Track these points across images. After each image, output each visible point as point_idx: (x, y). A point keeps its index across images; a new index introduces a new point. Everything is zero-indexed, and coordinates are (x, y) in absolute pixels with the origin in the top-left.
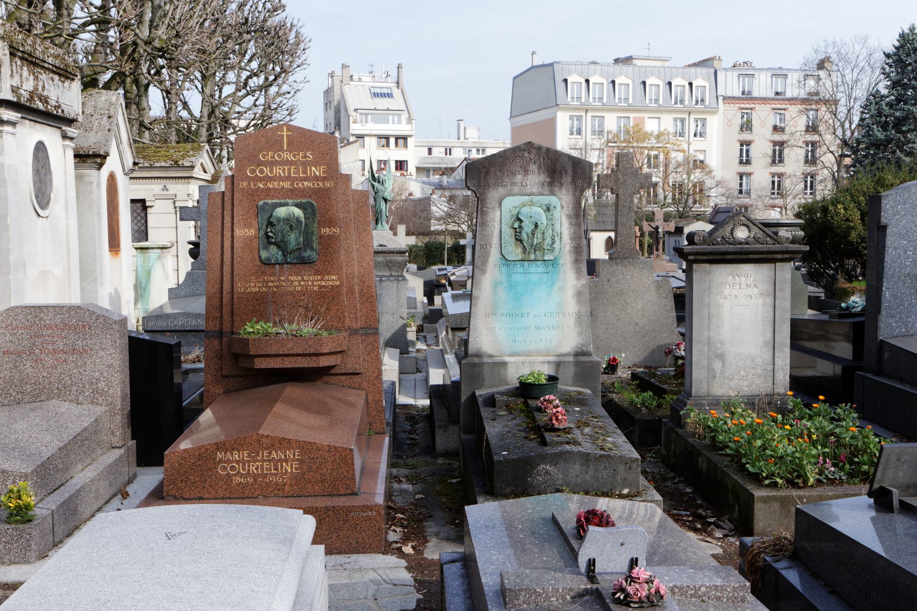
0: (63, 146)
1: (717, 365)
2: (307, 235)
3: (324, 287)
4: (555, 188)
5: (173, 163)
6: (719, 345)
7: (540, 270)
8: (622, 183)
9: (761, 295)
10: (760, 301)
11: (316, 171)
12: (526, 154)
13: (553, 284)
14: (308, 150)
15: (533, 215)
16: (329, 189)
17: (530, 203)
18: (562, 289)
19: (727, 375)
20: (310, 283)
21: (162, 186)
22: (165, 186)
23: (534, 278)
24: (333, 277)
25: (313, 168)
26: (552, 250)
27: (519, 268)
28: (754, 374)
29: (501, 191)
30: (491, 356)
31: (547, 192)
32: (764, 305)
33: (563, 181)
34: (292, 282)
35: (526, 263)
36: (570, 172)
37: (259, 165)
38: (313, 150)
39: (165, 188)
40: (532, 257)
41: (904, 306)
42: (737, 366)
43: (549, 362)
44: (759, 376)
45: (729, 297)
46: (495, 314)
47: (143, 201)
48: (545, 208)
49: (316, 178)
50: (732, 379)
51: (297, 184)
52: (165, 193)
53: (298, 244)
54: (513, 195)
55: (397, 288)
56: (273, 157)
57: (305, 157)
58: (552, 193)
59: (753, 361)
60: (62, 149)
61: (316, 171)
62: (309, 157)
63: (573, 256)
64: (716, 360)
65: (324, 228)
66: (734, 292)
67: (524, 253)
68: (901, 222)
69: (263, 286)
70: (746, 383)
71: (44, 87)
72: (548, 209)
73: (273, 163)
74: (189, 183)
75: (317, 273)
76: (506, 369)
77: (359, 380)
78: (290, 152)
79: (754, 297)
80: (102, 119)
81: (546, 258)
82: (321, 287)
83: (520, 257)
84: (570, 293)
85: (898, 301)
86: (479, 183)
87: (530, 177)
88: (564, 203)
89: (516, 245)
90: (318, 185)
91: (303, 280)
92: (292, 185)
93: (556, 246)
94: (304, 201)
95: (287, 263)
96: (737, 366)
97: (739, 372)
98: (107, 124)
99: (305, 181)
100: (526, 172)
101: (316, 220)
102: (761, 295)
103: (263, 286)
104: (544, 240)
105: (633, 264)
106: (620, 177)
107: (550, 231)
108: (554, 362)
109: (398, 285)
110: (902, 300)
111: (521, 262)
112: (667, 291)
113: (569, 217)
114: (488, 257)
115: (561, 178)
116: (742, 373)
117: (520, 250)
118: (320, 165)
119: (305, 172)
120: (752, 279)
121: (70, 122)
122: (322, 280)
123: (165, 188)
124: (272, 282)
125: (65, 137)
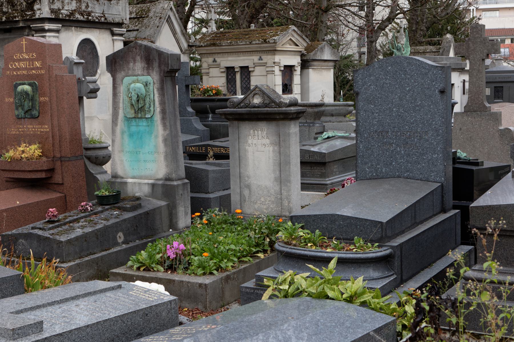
0: (113, 40)
1: (246, 192)
2: (32, 100)
3: (43, 132)
4: (150, 71)
5: (263, 41)
6: (247, 179)
7: (145, 124)
8: (473, 50)
9: (271, 144)
10: (271, 149)
11: (38, 64)
12: (134, 50)
13: (151, 133)
14: (34, 52)
15: (136, 89)
16: (43, 74)
17: (137, 81)
18: (156, 137)
19: (253, 200)
20: (36, 130)
21: (258, 57)
22: (261, 57)
23: (141, 129)
24: (46, 127)
25: (36, 63)
26: (149, 111)
27: (134, 123)
28: (269, 201)
29: (123, 73)
30: (123, 178)
31: (145, 74)
32: (274, 151)
33: (154, 66)
34: (29, 128)
35: (137, 120)
36: (157, 60)
37: (14, 62)
38: (36, 52)
39: (261, 59)
40: (140, 115)
41: (374, 156)
42: (258, 194)
43: (148, 184)
44: (273, 202)
45: (251, 145)
46: (123, 151)
47: (247, 67)
48: (145, 84)
49: (37, 68)
50: (256, 203)
51: (30, 72)
52: (215, 63)
53: (29, 107)
54: (129, 76)
55: (309, 131)
56: (19, 57)
57: (33, 56)
58: (149, 74)
59: (268, 191)
60: (112, 42)
61: (38, 64)
62: (34, 56)
63: (161, 115)
64: (245, 188)
65: (42, 97)
66: (255, 142)
67: (135, 113)
68: (369, 90)
69: (17, 131)
70: (265, 207)
71: (87, 6)
72: (147, 85)
73: (19, 60)
74: (275, 54)
75: (40, 124)
76: (126, 187)
77: (62, 188)
78: (27, 54)
79: (267, 146)
80: (156, 20)
81: (147, 116)
82: (41, 132)
83: (133, 116)
84: (160, 139)
85: (370, 152)
86: (112, 68)
87: (137, 64)
88: (155, 81)
89: (131, 108)
90: (38, 72)
91: (34, 128)
92: (28, 72)
93: (152, 108)
94: (32, 82)
95: (27, 118)
96: (258, 194)
97: (260, 198)
98: (158, 23)
99: (33, 70)
100: (135, 61)
101: (37, 93)
102: (271, 144)
103: (17, 131)
104: (145, 104)
105: (481, 116)
106: (471, 45)
107: (148, 99)
108: (151, 184)
109: (309, 130)
110: (372, 151)
111: (135, 119)
112: (509, 138)
113: (158, 90)
114: (118, 115)
115: (153, 64)
116: (262, 199)
117: (133, 111)
118: (39, 61)
119: (33, 65)
120: (265, 132)
121: (120, 25)
122: (41, 128)
123: (261, 59)
124: (21, 128)
125: (113, 34)
